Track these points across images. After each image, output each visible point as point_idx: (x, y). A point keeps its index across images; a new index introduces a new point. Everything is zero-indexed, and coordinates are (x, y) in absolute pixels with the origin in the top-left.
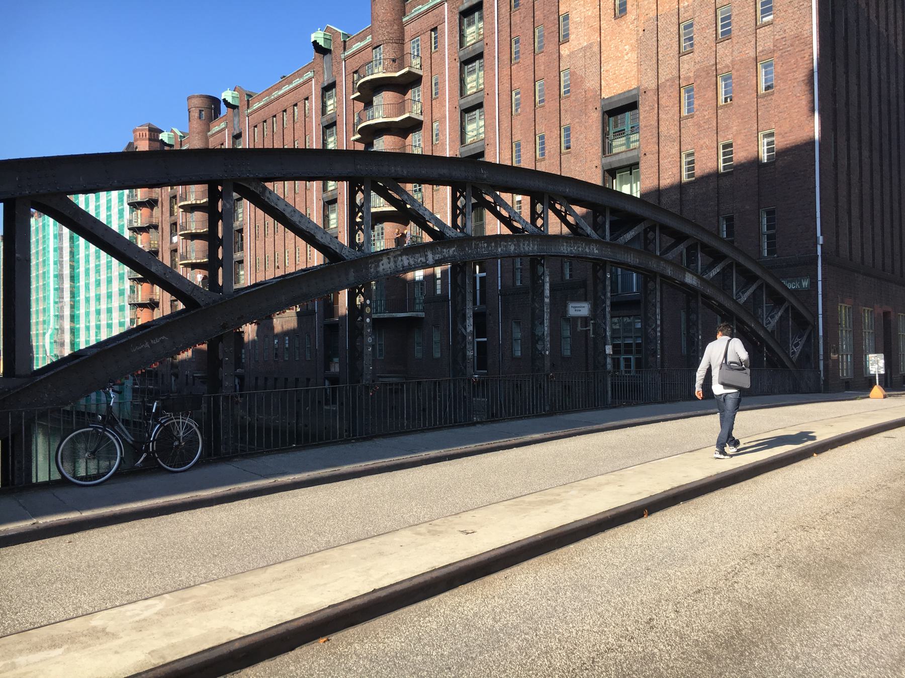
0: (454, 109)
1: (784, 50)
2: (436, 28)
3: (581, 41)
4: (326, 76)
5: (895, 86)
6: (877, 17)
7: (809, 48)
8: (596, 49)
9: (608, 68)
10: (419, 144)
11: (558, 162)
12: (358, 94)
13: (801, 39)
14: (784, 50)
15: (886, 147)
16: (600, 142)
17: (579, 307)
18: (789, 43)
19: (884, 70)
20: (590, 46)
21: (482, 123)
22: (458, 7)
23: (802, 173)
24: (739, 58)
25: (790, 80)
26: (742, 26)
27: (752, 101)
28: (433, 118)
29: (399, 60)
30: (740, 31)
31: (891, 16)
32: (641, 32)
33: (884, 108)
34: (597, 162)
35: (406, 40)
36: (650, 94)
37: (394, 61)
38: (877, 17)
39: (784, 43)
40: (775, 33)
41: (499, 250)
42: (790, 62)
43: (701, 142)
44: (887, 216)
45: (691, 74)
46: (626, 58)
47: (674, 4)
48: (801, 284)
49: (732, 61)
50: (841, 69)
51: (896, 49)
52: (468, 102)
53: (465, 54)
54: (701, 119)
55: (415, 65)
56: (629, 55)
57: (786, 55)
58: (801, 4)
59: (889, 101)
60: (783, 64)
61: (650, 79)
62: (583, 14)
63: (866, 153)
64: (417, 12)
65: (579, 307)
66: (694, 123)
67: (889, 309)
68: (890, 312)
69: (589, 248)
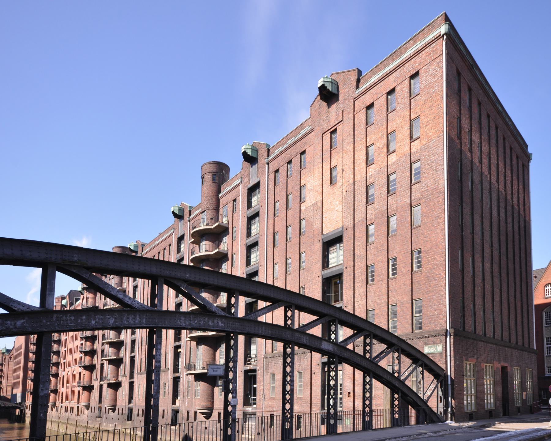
0: (243, 246)
1: (427, 198)
2: (236, 199)
3: (312, 201)
4: (180, 231)
5: (511, 225)
6: (498, 182)
7: (442, 195)
8: (320, 204)
9: (326, 216)
10: (225, 268)
11: (298, 275)
12: (193, 240)
13: (437, 190)
14: (427, 198)
15: (504, 262)
16: (321, 261)
17: (216, 368)
18: (430, 193)
19: (502, 214)
20: (316, 203)
21: (258, 254)
22: (247, 186)
23: (438, 276)
24: (400, 205)
25: (431, 216)
26: (402, 184)
27: (408, 231)
28: (233, 252)
29: (216, 217)
30: (401, 188)
31: (509, 183)
32: (345, 193)
33: (503, 238)
34: (319, 274)
35: (220, 208)
36: (349, 230)
37: (212, 219)
38: (498, 182)
39: (427, 193)
40: (422, 187)
41: (93, 322)
42: (430, 205)
43: (379, 258)
44: (505, 305)
45: (373, 217)
46: (336, 209)
47: (364, 174)
48: (436, 349)
49: (397, 207)
50: (467, 210)
51: (513, 203)
52: (251, 241)
53: (250, 213)
54: (378, 244)
55: (224, 220)
56: (338, 207)
57: (428, 201)
58: (438, 167)
59: (507, 234)
60: (426, 206)
61: (350, 221)
62: (313, 184)
63: (487, 265)
64: (227, 191)
65: (216, 368)
66: (374, 247)
67: (505, 365)
68: (507, 366)
69: (213, 322)
